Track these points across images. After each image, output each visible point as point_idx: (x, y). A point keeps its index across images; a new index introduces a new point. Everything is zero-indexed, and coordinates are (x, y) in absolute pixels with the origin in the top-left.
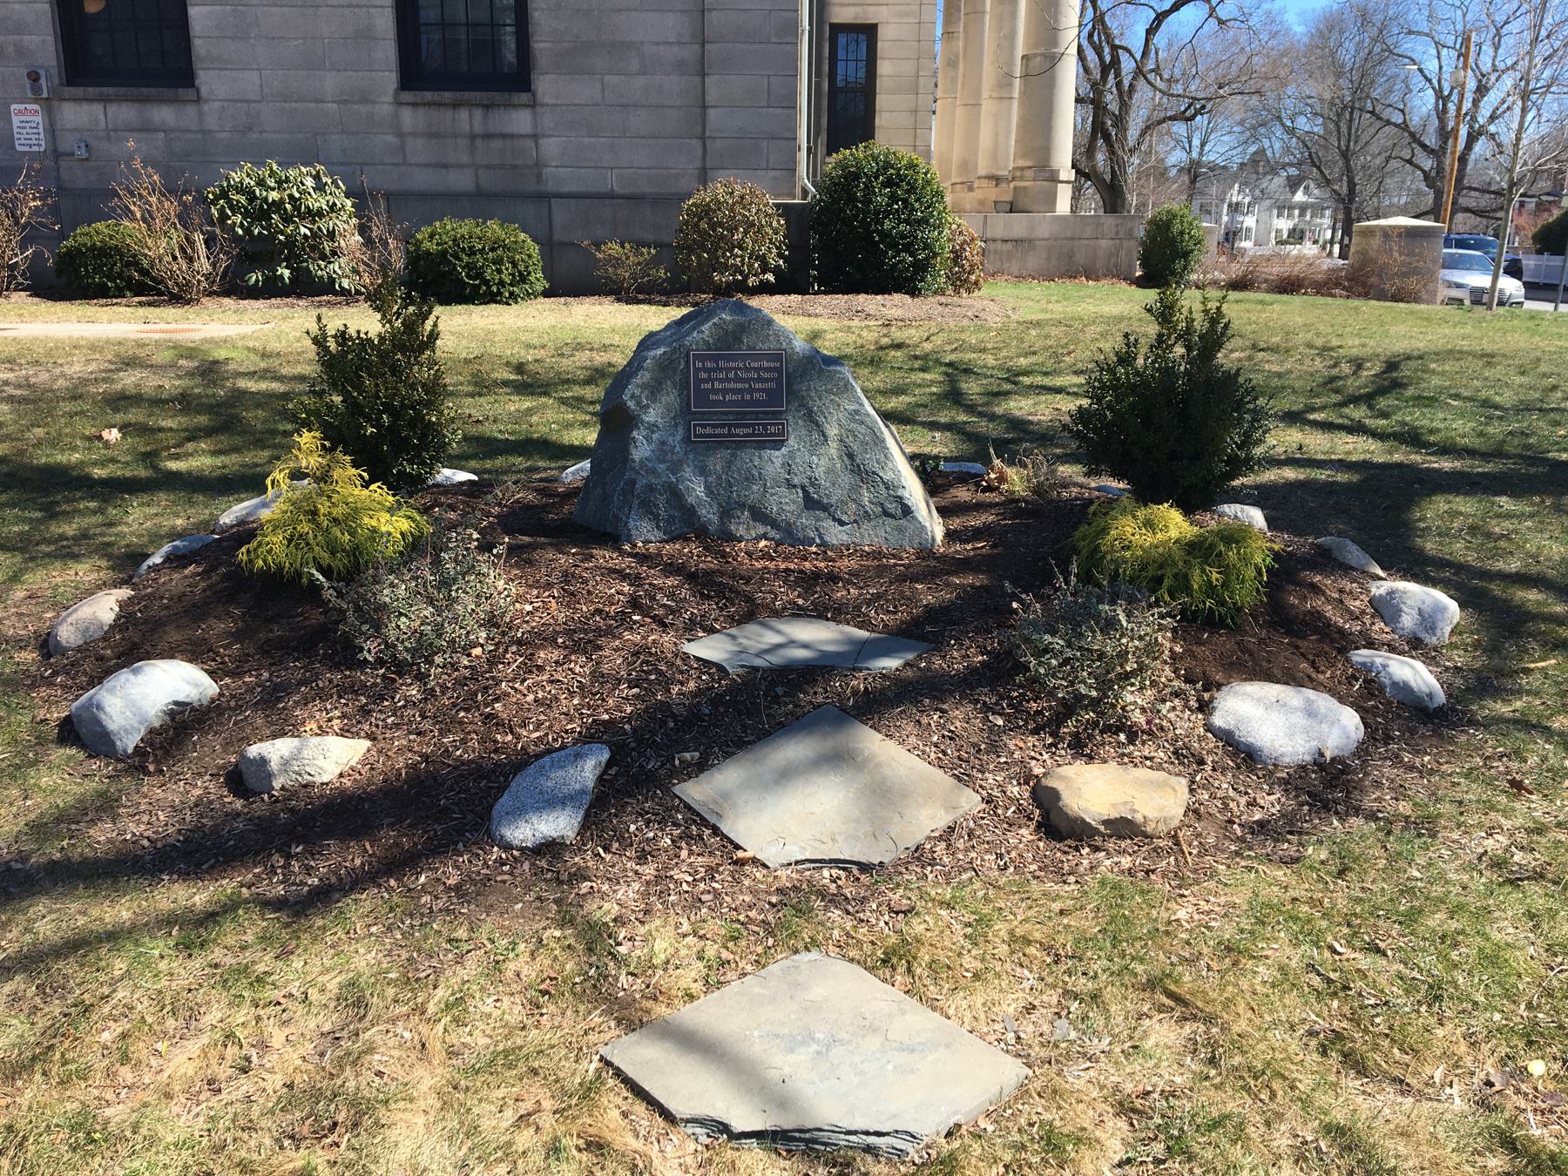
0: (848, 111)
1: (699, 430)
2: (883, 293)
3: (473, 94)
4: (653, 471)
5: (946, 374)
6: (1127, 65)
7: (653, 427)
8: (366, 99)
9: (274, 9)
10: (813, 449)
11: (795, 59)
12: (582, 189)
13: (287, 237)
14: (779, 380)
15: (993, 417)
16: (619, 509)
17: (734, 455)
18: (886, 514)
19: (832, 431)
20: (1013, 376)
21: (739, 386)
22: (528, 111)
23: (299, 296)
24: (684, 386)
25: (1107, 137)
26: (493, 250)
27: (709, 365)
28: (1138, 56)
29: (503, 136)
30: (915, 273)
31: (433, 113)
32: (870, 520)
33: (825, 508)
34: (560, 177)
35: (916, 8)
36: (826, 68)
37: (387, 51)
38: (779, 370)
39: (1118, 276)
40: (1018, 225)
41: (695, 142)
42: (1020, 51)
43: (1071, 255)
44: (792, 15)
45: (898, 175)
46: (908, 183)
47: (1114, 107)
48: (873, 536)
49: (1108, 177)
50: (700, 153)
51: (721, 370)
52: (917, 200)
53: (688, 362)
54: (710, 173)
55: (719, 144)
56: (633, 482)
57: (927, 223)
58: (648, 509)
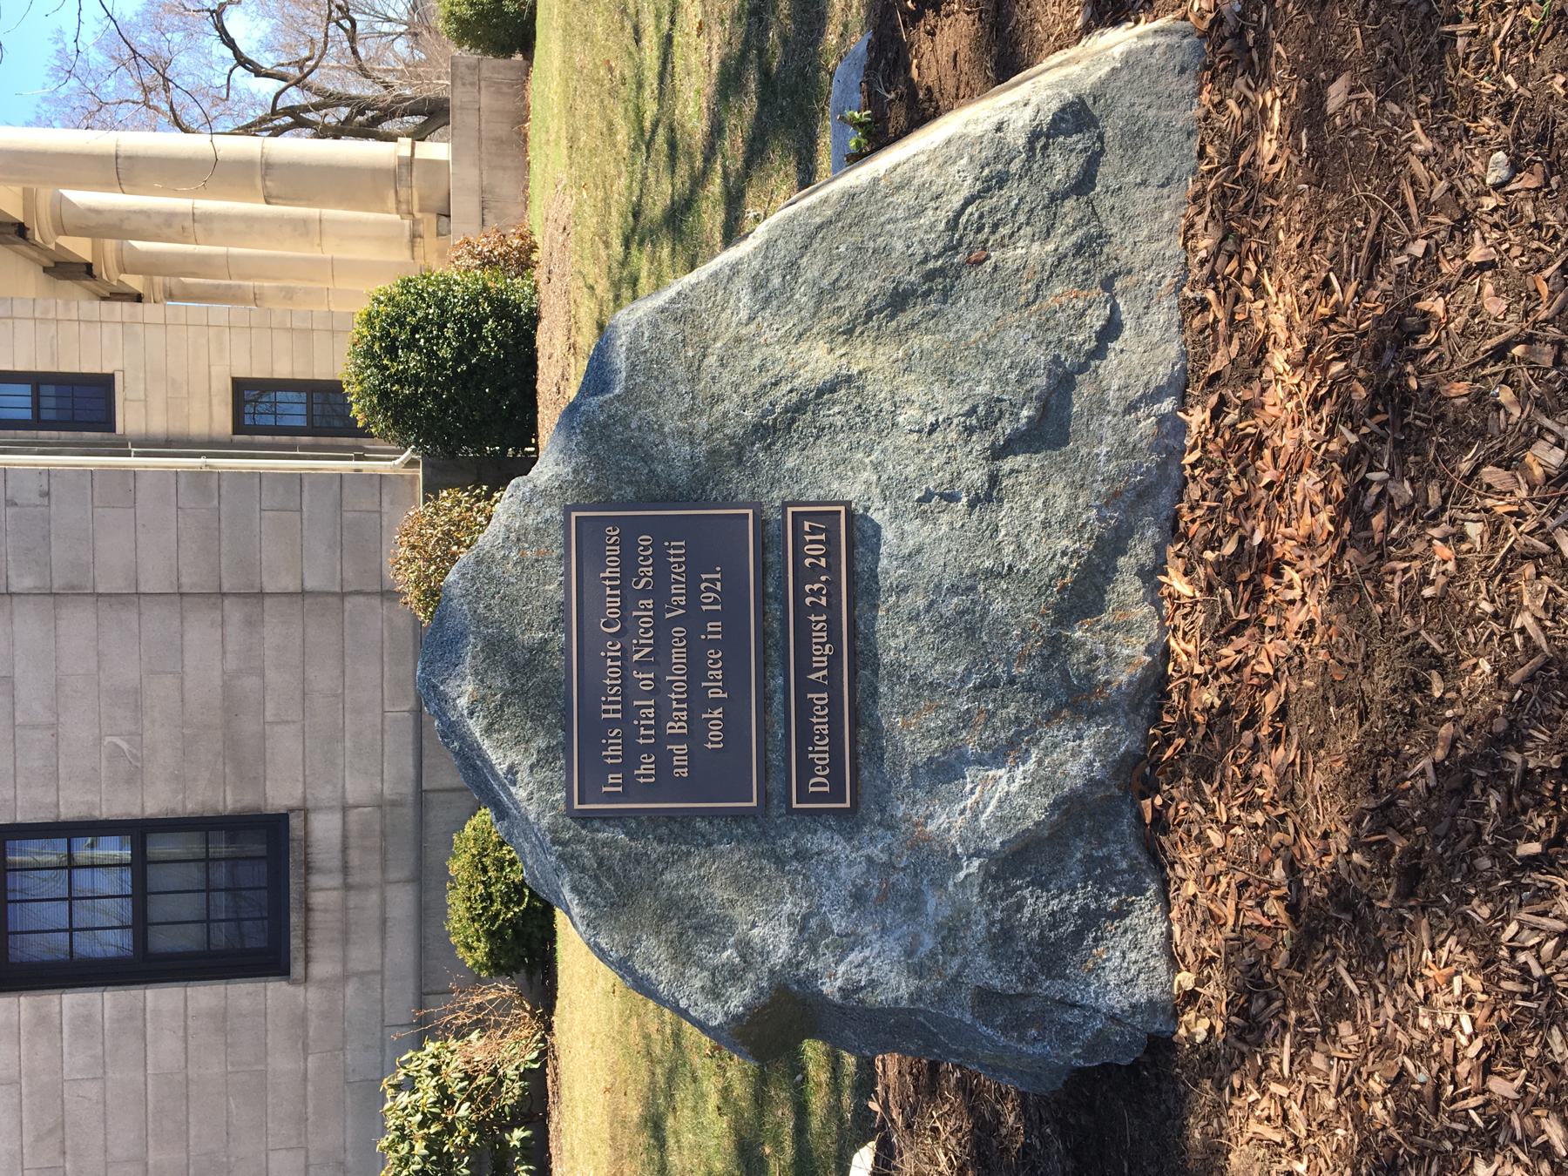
0: (319, 413)
1: (819, 781)
2: (536, 359)
3: (292, 887)
4: (950, 932)
5: (641, 243)
6: (295, 97)
7: (808, 932)
8: (302, 1020)
9: (192, 1133)
10: (872, 421)
11: (238, 475)
12: (410, 749)
13: (472, 1131)
14: (663, 531)
15: (717, 130)
16: (1066, 1038)
17: (895, 674)
18: (1083, 184)
19: (819, 360)
20: (643, 140)
21: (678, 655)
22: (312, 817)
23: (547, 1115)
24: (678, 829)
25: (376, 121)
26: (485, 870)
27: (613, 752)
28: (283, 84)
29: (345, 849)
30: (509, 317)
31: (316, 937)
32: (1102, 237)
33: (1063, 383)
34: (395, 778)
35: (212, 331)
36: (284, 439)
37: (242, 994)
38: (630, 530)
39: (524, 88)
40: (464, 208)
41: (347, 606)
42: (259, 208)
43: (499, 141)
44: (182, 480)
45: (381, 339)
46: (391, 325)
47: (344, 112)
48: (1155, 230)
49: (419, 120)
50: (361, 599)
51: (629, 712)
52: (413, 313)
53: (607, 818)
54: (386, 587)
55: (349, 575)
56: (986, 998)
57: (443, 299)
58: (1059, 951)
